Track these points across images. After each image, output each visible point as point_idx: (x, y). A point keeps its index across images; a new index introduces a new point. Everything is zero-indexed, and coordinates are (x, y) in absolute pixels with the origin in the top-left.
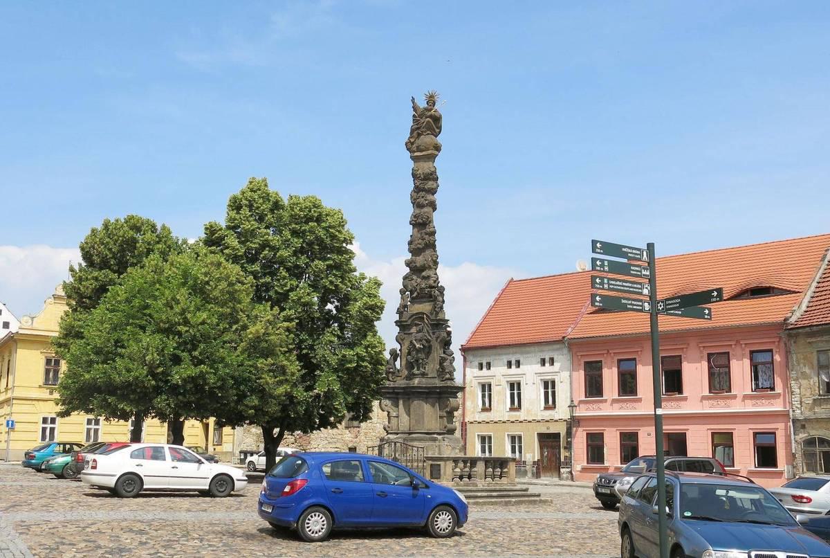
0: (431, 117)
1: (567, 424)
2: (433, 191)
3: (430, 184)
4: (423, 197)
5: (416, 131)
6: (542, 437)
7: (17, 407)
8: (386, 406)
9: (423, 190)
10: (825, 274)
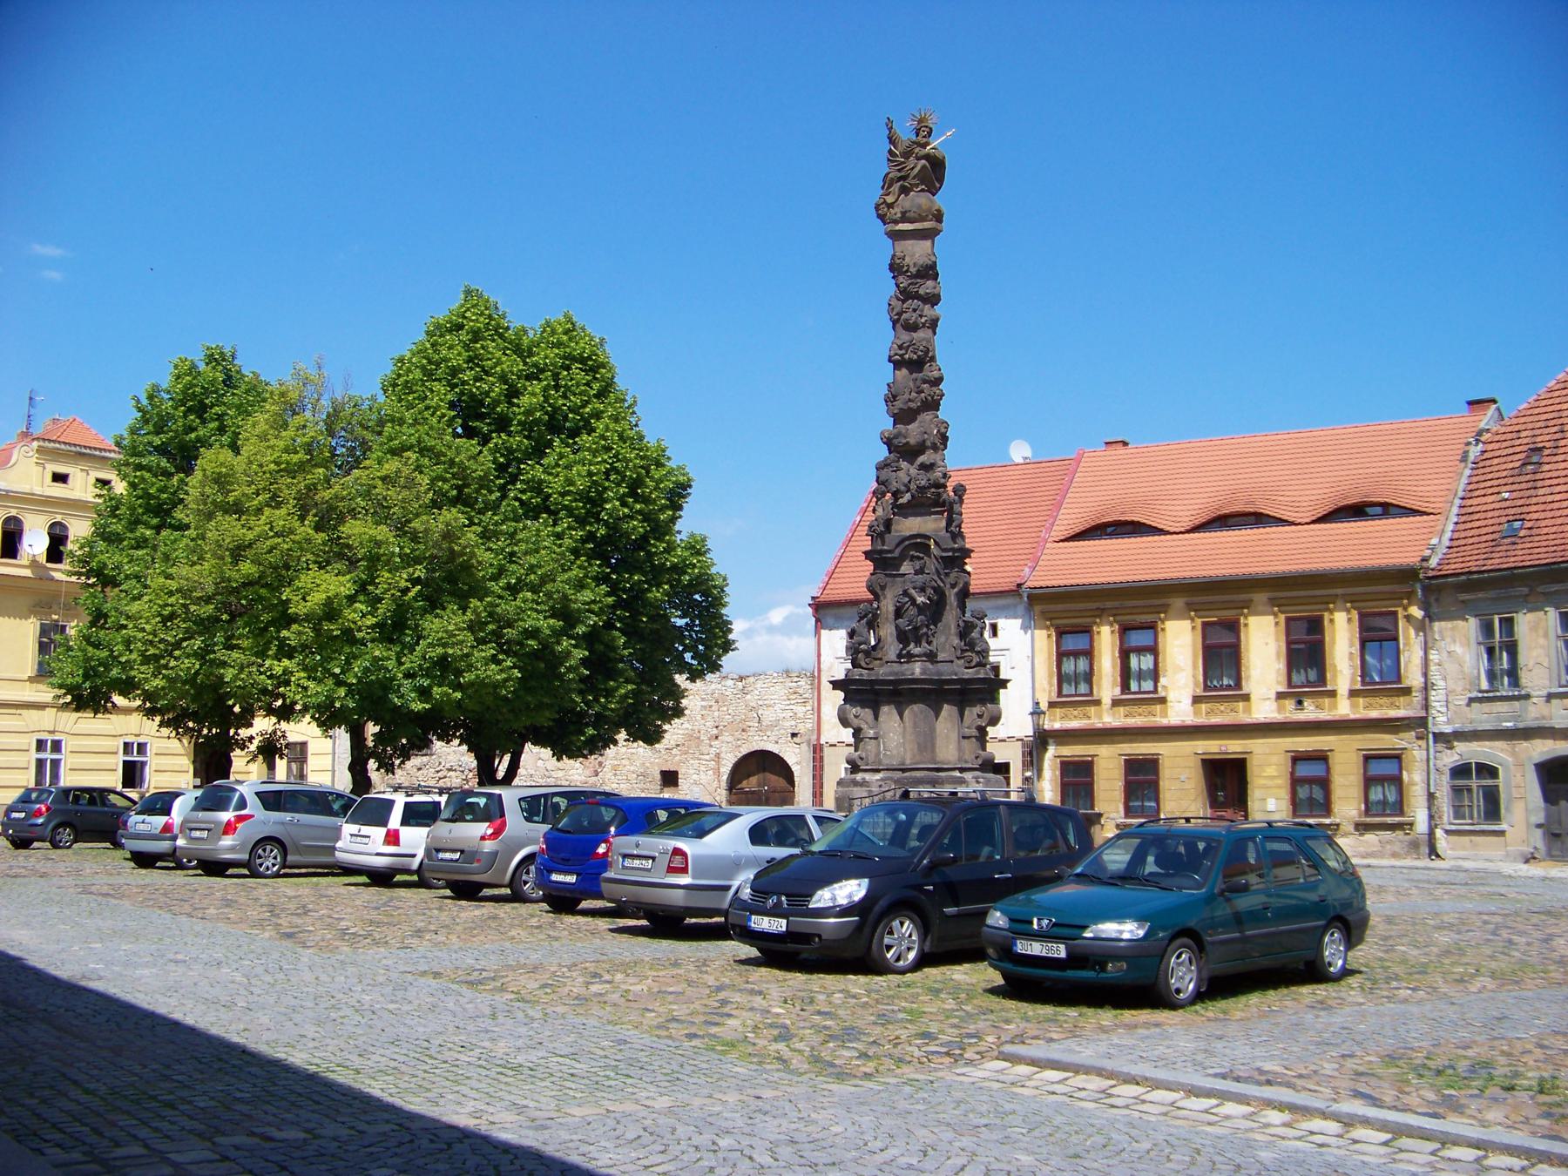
0: (927, 157)
1: (1023, 746)
2: (934, 300)
3: (927, 287)
4: (915, 310)
5: (898, 181)
8: (856, 717)
9: (917, 296)
10: (1470, 484)
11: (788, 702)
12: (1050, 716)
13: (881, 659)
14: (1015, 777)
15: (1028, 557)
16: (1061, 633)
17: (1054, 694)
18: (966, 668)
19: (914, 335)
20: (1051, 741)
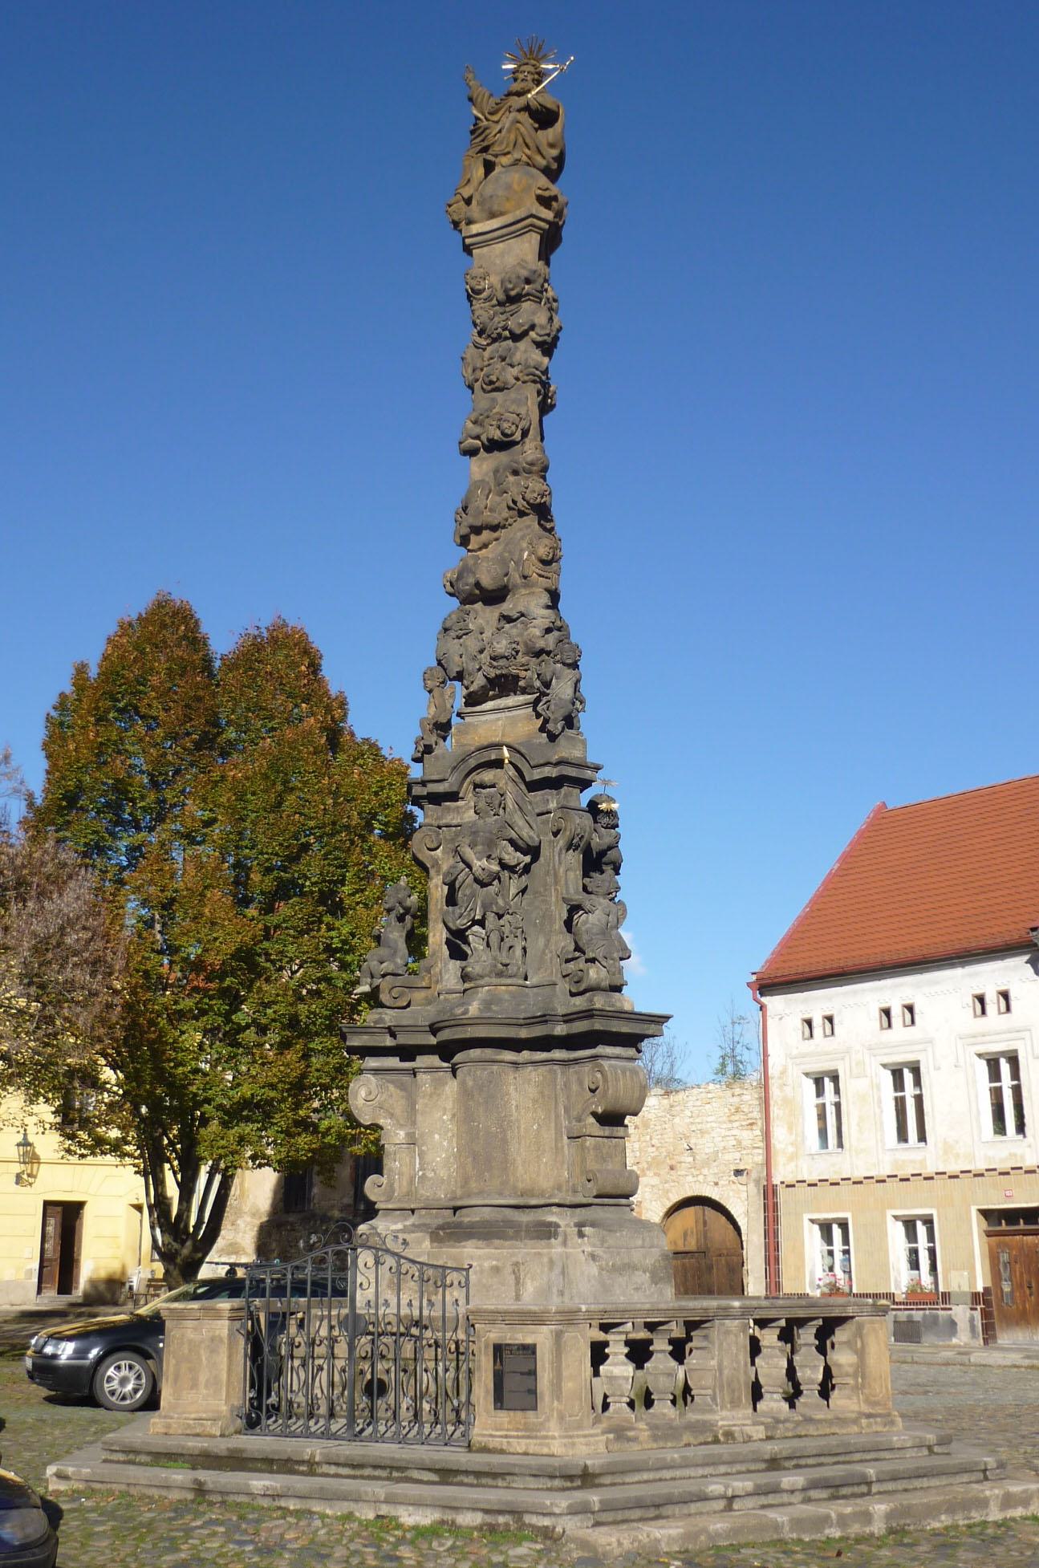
7: (776, 1181)
18: (573, 995)
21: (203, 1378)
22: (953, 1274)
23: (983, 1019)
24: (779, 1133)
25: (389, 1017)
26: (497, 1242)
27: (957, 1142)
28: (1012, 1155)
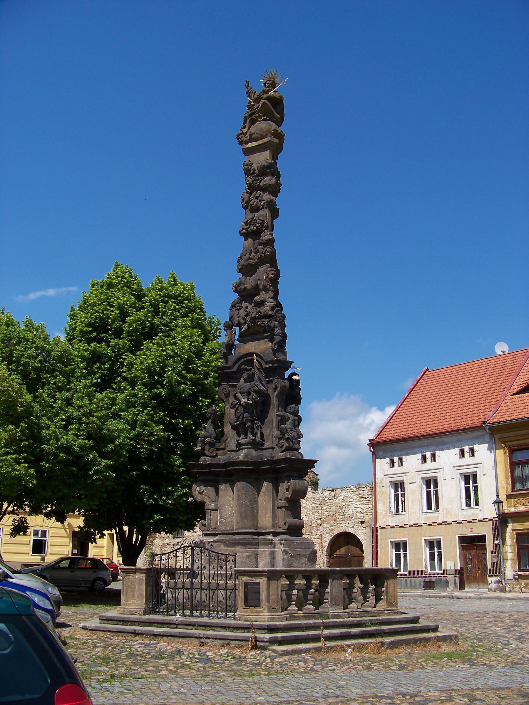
1: (493, 524)
6: (463, 540)
8: (200, 493)
9: (259, 189)
11: (359, 503)
12: (508, 504)
13: (224, 449)
14: (489, 545)
15: (493, 406)
16: (512, 451)
17: (510, 490)
19: (256, 214)
20: (509, 520)
21: (136, 594)
22: (448, 562)
23: (464, 459)
24: (379, 506)
25: (208, 460)
26: (249, 546)
27: (451, 509)
28: (473, 514)
